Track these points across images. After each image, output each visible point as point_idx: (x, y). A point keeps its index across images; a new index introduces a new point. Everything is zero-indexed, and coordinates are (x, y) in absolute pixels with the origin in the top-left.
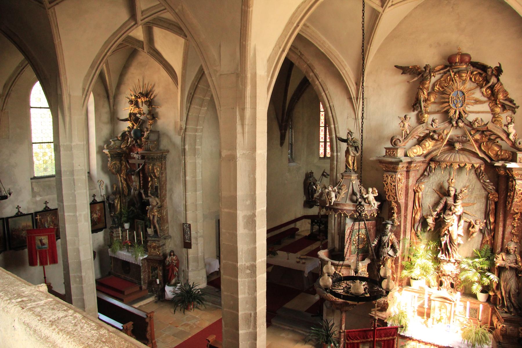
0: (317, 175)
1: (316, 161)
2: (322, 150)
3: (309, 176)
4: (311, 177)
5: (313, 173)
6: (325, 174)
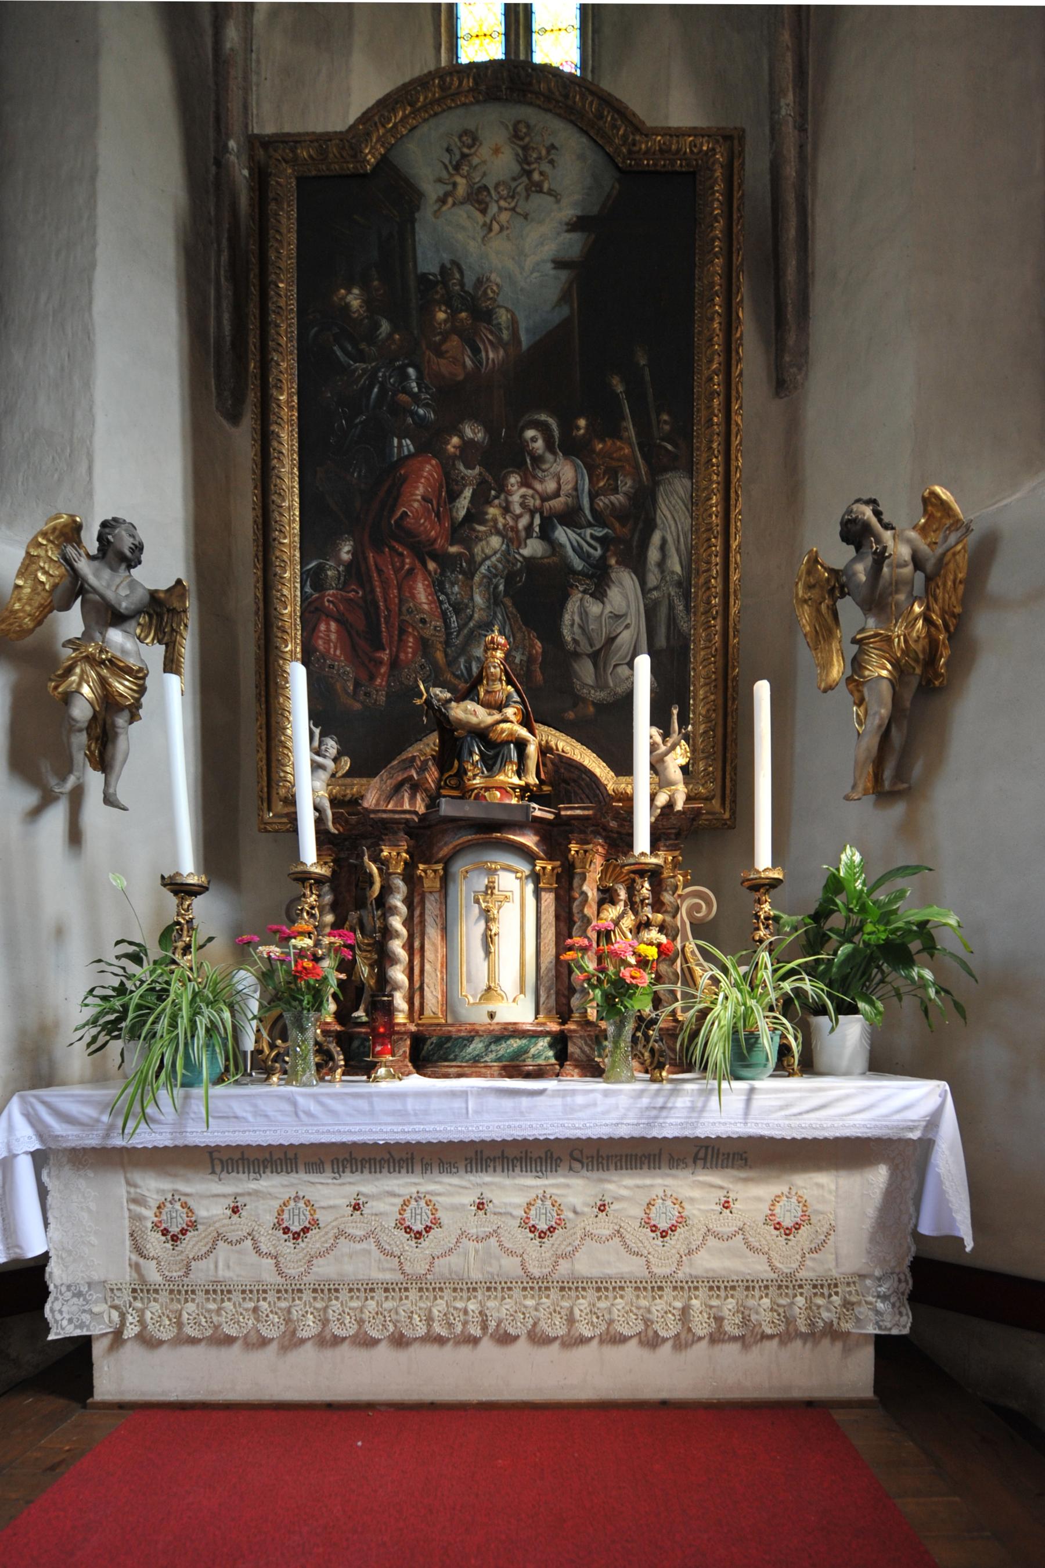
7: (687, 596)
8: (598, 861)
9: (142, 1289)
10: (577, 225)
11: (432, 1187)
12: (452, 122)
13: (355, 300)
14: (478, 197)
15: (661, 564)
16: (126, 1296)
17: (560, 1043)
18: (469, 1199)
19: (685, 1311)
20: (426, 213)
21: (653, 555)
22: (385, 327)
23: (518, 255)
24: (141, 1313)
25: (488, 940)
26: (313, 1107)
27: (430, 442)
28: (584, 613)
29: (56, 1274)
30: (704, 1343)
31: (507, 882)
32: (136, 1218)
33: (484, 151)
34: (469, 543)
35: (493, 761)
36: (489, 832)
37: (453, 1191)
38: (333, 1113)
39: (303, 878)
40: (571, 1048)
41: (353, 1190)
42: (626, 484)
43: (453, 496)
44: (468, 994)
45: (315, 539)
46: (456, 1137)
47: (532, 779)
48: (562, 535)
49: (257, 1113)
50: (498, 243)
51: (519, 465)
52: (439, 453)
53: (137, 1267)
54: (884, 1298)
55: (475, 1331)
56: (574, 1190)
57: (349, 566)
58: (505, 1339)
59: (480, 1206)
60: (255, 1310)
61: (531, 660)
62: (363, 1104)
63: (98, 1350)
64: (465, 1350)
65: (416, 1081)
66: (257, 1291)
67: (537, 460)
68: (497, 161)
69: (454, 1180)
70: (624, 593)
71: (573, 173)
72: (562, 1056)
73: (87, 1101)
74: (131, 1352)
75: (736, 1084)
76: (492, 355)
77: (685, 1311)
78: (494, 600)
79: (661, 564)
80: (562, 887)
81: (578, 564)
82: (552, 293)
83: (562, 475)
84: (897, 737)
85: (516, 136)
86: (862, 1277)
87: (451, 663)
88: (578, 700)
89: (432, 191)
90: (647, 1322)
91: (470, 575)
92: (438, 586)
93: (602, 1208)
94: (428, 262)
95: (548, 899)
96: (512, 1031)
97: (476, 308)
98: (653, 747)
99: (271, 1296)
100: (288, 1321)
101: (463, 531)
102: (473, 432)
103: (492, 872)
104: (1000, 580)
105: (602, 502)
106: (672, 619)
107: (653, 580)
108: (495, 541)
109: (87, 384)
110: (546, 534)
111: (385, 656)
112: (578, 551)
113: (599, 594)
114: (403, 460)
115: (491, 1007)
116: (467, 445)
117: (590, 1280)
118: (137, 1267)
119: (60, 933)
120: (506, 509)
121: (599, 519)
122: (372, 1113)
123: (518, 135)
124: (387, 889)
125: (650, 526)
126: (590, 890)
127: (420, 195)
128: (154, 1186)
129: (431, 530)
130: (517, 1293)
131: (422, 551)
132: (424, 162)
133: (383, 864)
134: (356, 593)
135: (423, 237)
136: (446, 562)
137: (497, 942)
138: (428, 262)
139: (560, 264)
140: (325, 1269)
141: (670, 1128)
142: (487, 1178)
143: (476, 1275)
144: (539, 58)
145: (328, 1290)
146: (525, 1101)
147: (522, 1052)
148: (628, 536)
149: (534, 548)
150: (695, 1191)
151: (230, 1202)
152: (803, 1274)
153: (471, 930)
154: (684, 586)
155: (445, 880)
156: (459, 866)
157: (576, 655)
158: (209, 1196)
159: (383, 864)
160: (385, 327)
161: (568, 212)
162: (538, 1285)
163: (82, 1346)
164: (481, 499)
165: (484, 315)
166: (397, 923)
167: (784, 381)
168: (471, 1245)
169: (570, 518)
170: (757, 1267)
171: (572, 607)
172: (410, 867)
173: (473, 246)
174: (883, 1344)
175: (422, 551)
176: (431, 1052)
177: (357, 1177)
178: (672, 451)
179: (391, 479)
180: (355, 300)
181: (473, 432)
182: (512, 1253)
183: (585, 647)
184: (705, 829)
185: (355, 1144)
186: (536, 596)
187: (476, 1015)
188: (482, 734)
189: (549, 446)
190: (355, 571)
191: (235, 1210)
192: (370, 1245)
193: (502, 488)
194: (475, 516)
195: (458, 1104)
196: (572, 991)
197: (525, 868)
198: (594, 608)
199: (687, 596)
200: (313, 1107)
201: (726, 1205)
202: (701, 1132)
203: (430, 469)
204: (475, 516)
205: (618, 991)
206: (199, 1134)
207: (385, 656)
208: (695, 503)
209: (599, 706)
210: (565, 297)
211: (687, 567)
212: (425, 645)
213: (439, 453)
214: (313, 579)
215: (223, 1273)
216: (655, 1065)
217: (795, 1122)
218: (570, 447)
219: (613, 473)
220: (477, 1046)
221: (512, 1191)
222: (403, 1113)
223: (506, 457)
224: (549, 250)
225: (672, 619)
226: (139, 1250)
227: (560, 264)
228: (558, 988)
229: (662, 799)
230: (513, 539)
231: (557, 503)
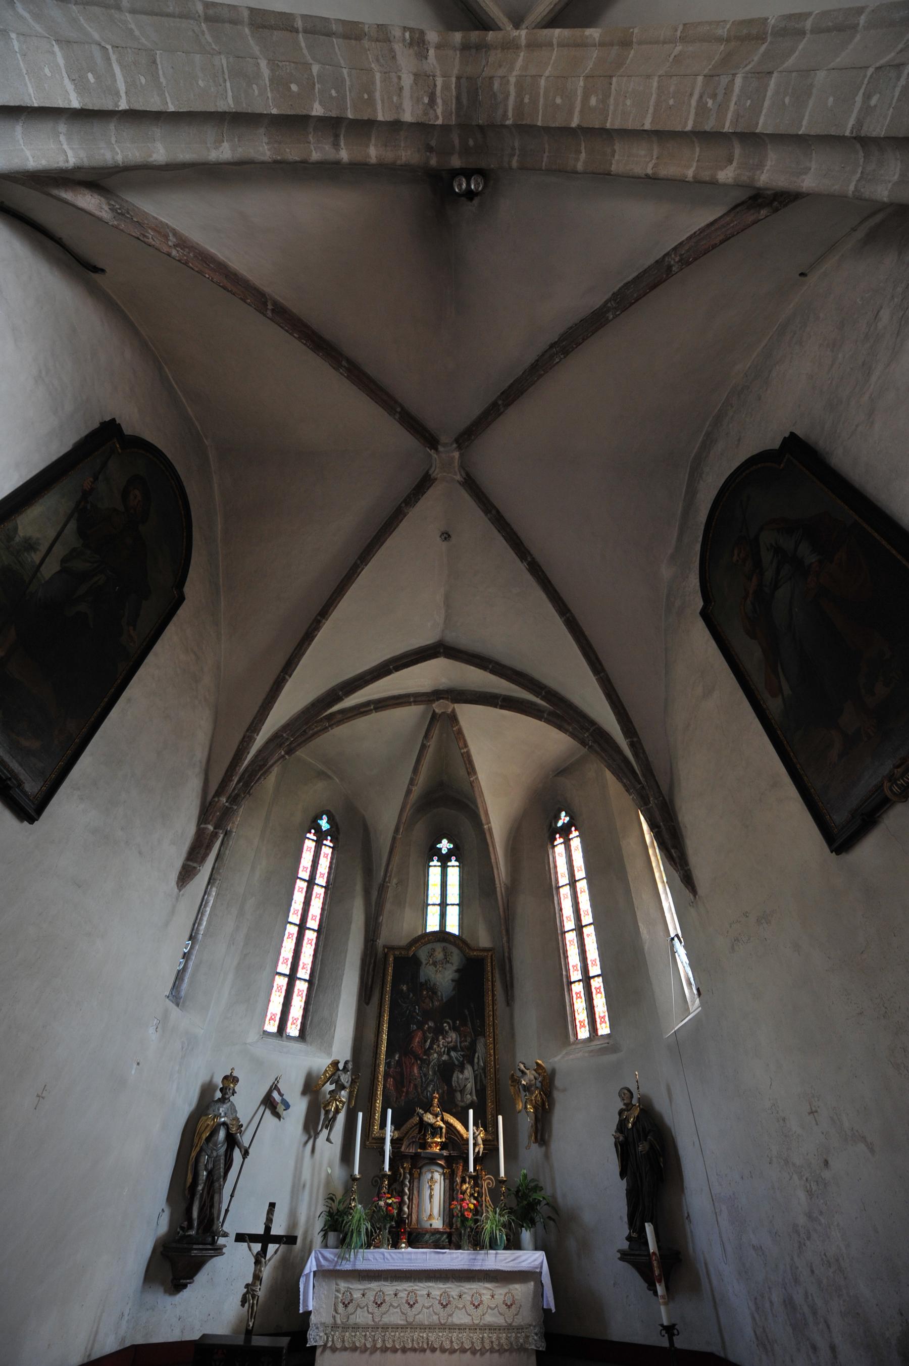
0: (245, 1102)
1: (253, 1036)
2: (275, 1006)
3: (214, 1096)
4: (223, 1100)
5: (235, 1080)
6: (275, 1095)
7: (485, 1073)
8: (461, 1168)
9: (335, 1326)
10: (457, 971)
11: (416, 1288)
12: (429, 946)
13: (405, 988)
14: (435, 964)
15: (478, 1063)
16: (329, 1329)
17: (450, 1235)
18: (425, 1292)
19: (483, 1338)
20: (423, 966)
21: (476, 1060)
22: (411, 995)
23: (443, 977)
24: (333, 1336)
25: (431, 1196)
26: (389, 1257)
27: (420, 1026)
28: (458, 1078)
29: (313, 1319)
30: (488, 1354)
31: (437, 1176)
32: (337, 1297)
33: (436, 953)
34: (428, 1056)
35: (434, 1135)
36: (432, 1160)
37: (421, 1288)
38: (393, 1259)
39: (385, 1175)
40: (453, 1239)
41: (395, 1288)
42: (469, 1039)
43: (426, 1042)
44: (425, 1217)
45: (389, 1054)
46: (424, 1268)
47: (444, 1140)
48: (453, 1054)
49: (375, 1259)
50: (439, 975)
51: (442, 1034)
52: (423, 1030)
53: (334, 1317)
54: (536, 1334)
55: (425, 1346)
56: (453, 1289)
57: (398, 1061)
58: (433, 1350)
59: (428, 1295)
60: (365, 1335)
61: (444, 1092)
62: (400, 1256)
63: (318, 1351)
64: (422, 1354)
65: (410, 1249)
66: (366, 1328)
67: (447, 1032)
68: (439, 955)
69: (421, 1285)
70: (468, 1072)
71: (456, 958)
72: (450, 1242)
73: (331, 1253)
74: (328, 1353)
75: (491, 1251)
76: (436, 1003)
77: (483, 1338)
78: (434, 1073)
79: (478, 1063)
80: (450, 1178)
81: (456, 1063)
82: (451, 988)
83: (453, 1036)
84: (539, 1127)
85: (444, 950)
86: (530, 1325)
87: (422, 1093)
88: (456, 1105)
89: (424, 962)
90: (473, 1343)
91: (428, 1065)
92: (420, 1068)
93: (460, 1297)
94: (422, 980)
95: (447, 1181)
96: (436, 1232)
97: (433, 990)
98: (474, 1133)
99: (370, 1330)
100: (374, 1340)
101: (427, 1052)
102: (431, 1024)
103: (433, 1172)
104: (558, 1083)
105: (463, 1044)
106: (481, 1081)
107: (476, 1068)
108: (435, 1055)
109: (337, 1006)
110: (448, 1054)
111: (405, 1090)
112: (456, 1058)
113: (462, 1072)
114: (413, 1031)
115: (430, 1222)
116: (429, 1027)
117: (457, 1325)
118: (334, 1317)
119: (304, 1186)
120: (439, 1046)
121: (462, 1050)
122: (403, 1259)
123: (444, 949)
124: (405, 1178)
125: (475, 1052)
126: (458, 1180)
127: (421, 963)
128: (343, 1285)
129: (420, 1052)
130: (437, 1330)
131: (417, 1057)
132: (423, 954)
133: (404, 1169)
134: (399, 1070)
135: (422, 973)
136: (421, 1059)
137: (432, 1200)
138: (422, 980)
139: (453, 981)
140: (386, 1319)
141: (477, 1267)
142: (430, 1284)
143: (426, 1323)
144: (447, 930)
145: (385, 1328)
146: (441, 1255)
147: (439, 1239)
148: (469, 1056)
149: (445, 1057)
150: (485, 1290)
151: (362, 1292)
152: (514, 1324)
153: (427, 1193)
154: (484, 1069)
155: (420, 1174)
156: (424, 1170)
157: (456, 1091)
158: (357, 1288)
159: (404, 1169)
160: (411, 995)
161: (455, 968)
162: (443, 1327)
163: (314, 1348)
164: (432, 1043)
165: (435, 993)
166: (406, 1190)
167: (509, 1000)
168: (425, 1310)
169: (454, 1049)
170: (501, 1321)
171: (455, 1075)
172: (411, 1170)
173: (433, 976)
174: (538, 1353)
175: (417, 1057)
176: (415, 1240)
177: (396, 1283)
178: (480, 1032)
179: (410, 1037)
180: (405, 988)
181: (431, 1024)
182: (436, 1314)
183: (458, 1089)
184: (487, 1157)
185: (398, 1270)
186: (446, 1071)
187: (426, 1225)
188: (431, 1125)
189: (450, 1028)
190: (399, 1063)
191: (363, 1295)
192: (398, 1310)
193: (438, 1040)
194: (431, 1047)
195: (424, 1256)
196: (453, 1216)
197: (441, 1170)
198: (461, 1076)
199: (485, 1073)
200: (389, 1257)
201: (493, 1297)
202: (484, 1268)
203: (420, 1034)
204: (431, 1047)
205: (464, 1219)
206: (361, 1265)
207: (405, 1090)
208: (486, 1045)
209: (462, 1107)
210: (454, 989)
211: (484, 1063)
212: (416, 1086)
213: (423, 1030)
214: (388, 1065)
215: (358, 1320)
216: (412, 1244)
217: (508, 1265)
218: (455, 1029)
219: (465, 1037)
220: (427, 1236)
221: (437, 1289)
222: (410, 1259)
223: (439, 1031)
224: (450, 977)
225: (481, 1081)
226: (336, 1311)
227: (453, 981)
228: (449, 1215)
229: (477, 1150)
230: (440, 1055)
231: (451, 1045)
